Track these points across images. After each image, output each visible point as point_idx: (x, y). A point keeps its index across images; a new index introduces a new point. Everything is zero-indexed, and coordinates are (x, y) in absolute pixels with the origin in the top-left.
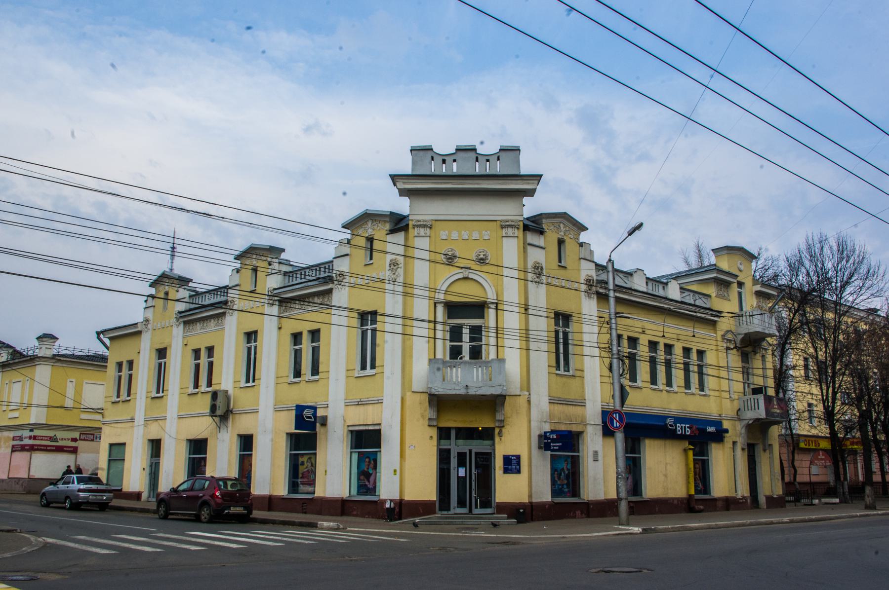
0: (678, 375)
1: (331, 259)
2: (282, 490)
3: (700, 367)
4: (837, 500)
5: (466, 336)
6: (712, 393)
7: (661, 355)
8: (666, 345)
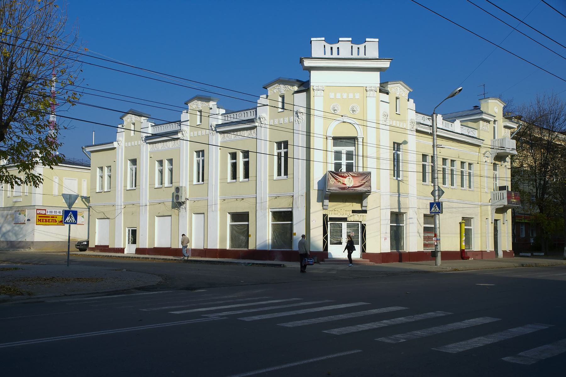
0: (457, 179)
1: (400, 142)
2: (386, 247)
3: (452, 170)
4: (543, 254)
5: (344, 156)
6: (475, 189)
7: (448, 166)
8: (451, 160)
